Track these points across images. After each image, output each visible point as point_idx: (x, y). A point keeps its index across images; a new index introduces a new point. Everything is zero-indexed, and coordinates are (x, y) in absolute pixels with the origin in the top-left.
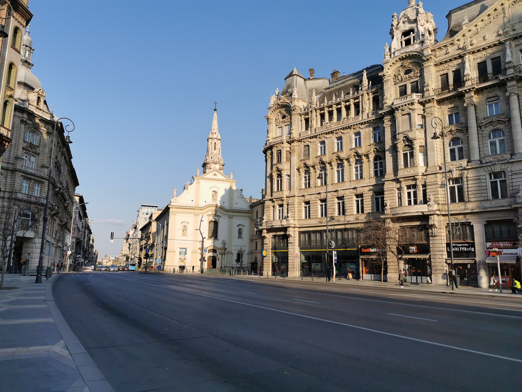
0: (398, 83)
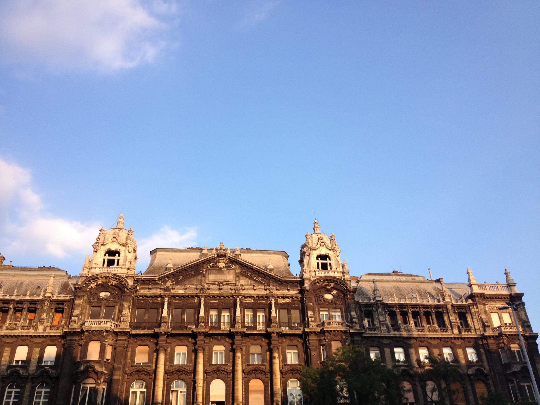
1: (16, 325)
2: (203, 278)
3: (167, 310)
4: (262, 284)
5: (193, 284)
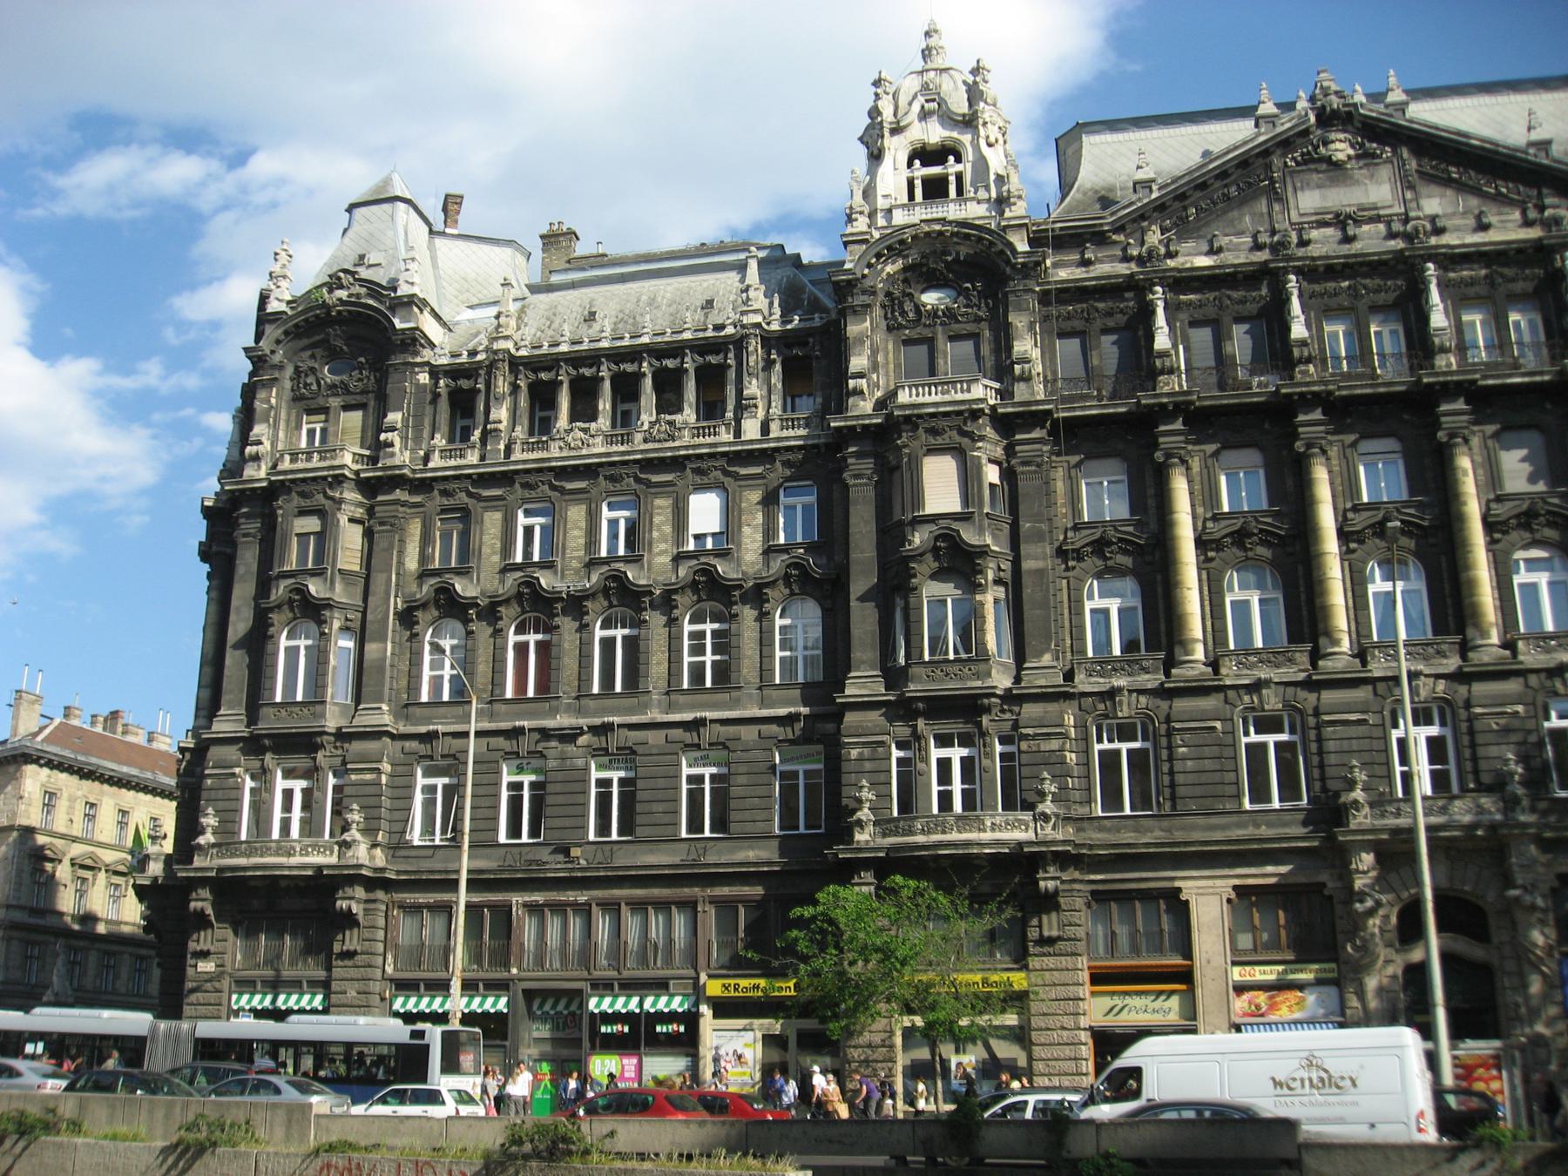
0: (900, 327)
1: (671, 423)
2: (1277, 207)
3: (1166, 330)
4: (1511, 203)
5: (1240, 234)
